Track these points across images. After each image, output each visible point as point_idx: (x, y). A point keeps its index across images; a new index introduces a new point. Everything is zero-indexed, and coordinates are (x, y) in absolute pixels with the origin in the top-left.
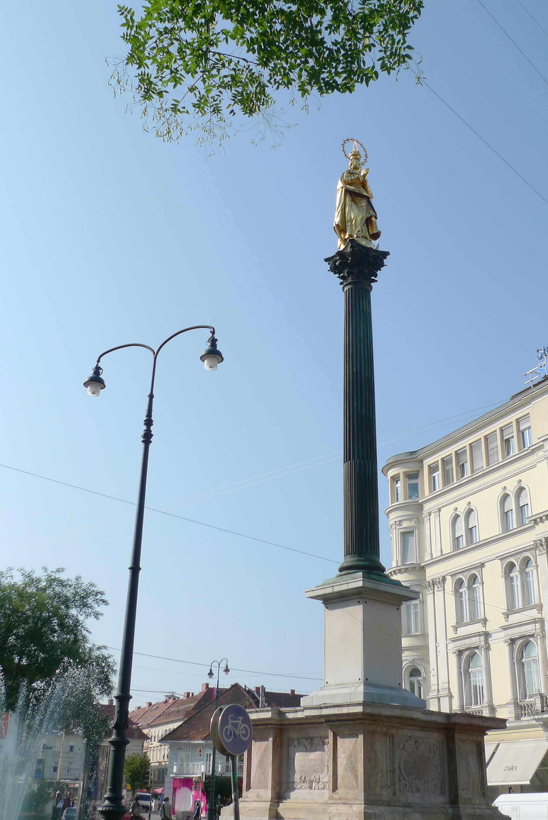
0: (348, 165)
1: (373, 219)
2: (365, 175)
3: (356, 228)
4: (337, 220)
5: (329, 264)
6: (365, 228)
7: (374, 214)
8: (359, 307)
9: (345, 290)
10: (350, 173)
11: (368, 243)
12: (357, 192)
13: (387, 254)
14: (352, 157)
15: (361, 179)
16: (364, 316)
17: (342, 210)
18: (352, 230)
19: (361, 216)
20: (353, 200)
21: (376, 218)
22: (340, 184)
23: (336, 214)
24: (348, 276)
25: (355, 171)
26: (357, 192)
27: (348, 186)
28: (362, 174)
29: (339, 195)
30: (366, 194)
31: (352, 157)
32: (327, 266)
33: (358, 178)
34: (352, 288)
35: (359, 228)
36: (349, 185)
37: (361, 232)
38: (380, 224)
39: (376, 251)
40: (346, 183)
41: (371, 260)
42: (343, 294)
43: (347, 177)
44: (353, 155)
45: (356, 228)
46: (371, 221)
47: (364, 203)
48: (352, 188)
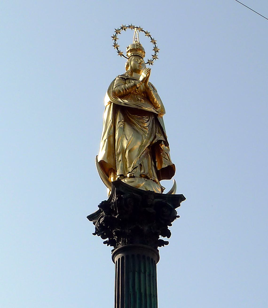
0: (121, 67)
1: (163, 146)
2: (146, 80)
3: (131, 163)
4: (101, 155)
5: (94, 224)
6: (147, 162)
7: (162, 138)
8: (134, 287)
9: (116, 259)
10: (124, 79)
11: (149, 185)
12: (135, 105)
13: (181, 198)
14: (129, 54)
15: (142, 87)
16: (140, 299)
17: (109, 138)
18: (125, 169)
19: (139, 143)
20: (127, 121)
21: (167, 144)
22: (107, 99)
23: (102, 143)
24: (119, 240)
25: (134, 75)
26: (135, 105)
27: (120, 100)
28: (141, 79)
29: (106, 115)
30: (149, 108)
31: (129, 54)
32: (92, 227)
33: (135, 85)
34: (123, 258)
35: (135, 162)
36: (121, 97)
37: (138, 169)
38: (175, 154)
39: (160, 196)
40: (115, 94)
41: (152, 210)
42: (113, 266)
43: (118, 85)
44: (131, 51)
45: (131, 163)
46: (160, 150)
47: (147, 123)
48: (126, 101)
